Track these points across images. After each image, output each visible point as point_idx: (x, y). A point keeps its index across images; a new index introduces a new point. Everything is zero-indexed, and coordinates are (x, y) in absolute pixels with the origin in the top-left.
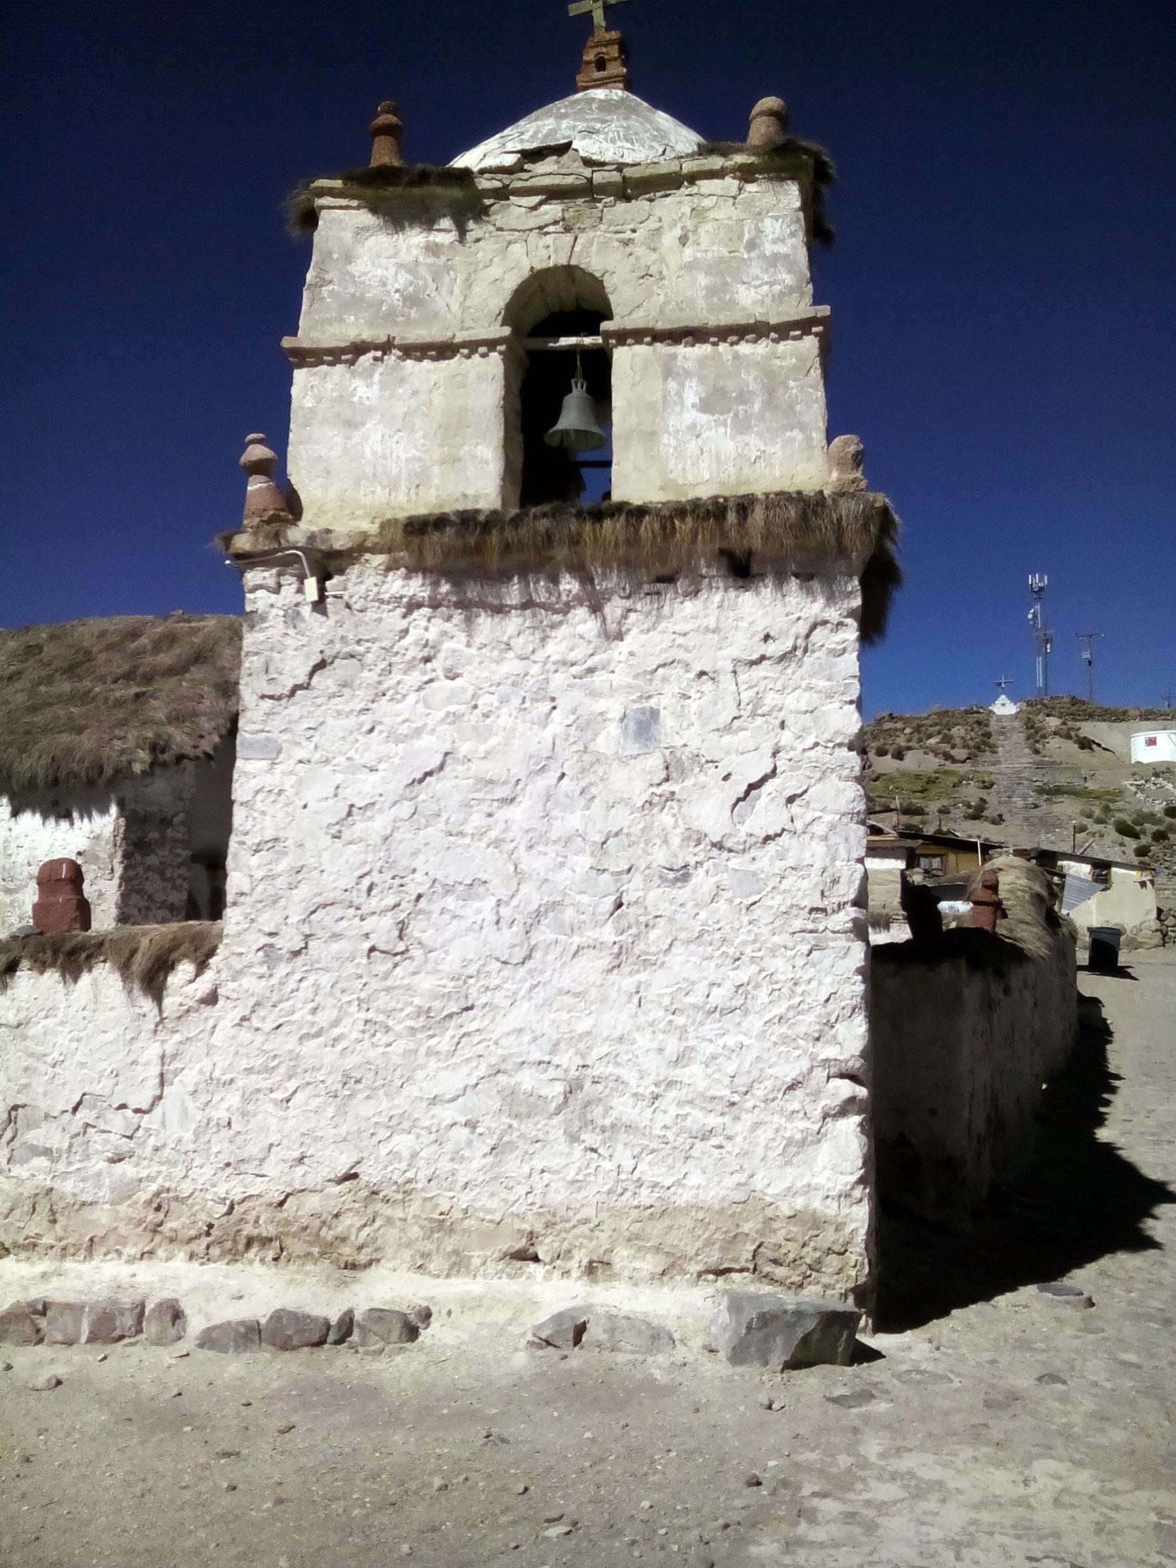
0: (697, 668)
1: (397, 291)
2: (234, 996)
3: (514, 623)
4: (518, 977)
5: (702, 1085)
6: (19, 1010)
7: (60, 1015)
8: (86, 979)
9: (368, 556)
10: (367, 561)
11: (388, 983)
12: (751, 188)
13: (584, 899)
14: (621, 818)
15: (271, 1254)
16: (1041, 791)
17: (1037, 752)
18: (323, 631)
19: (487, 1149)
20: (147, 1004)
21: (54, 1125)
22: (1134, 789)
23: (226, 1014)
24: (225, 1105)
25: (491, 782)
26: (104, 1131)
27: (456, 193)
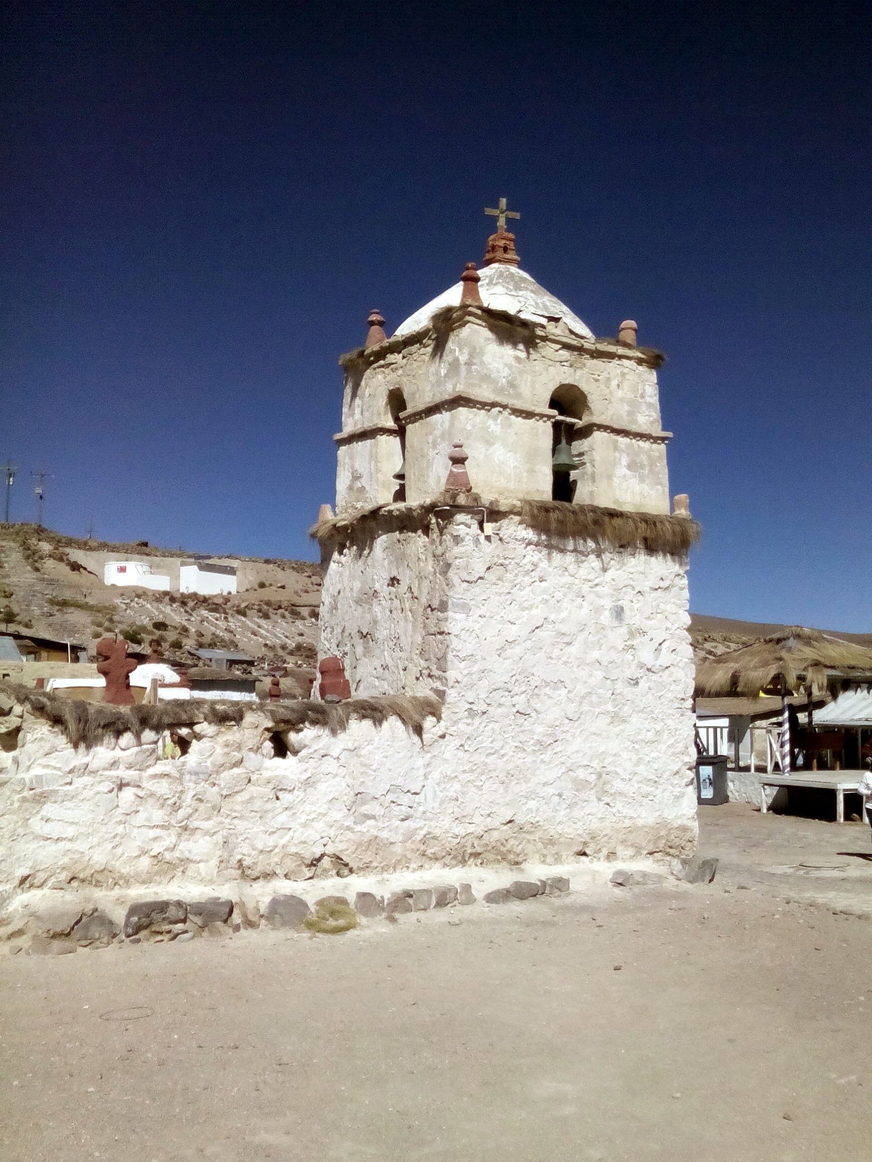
0: (637, 589)
1: (504, 377)
2: (455, 734)
3: (570, 558)
4: (576, 726)
5: (645, 774)
6: (355, 741)
7: (376, 744)
8: (385, 724)
9: (512, 516)
10: (511, 518)
11: (522, 728)
12: (640, 368)
13: (601, 691)
14: (614, 656)
15: (479, 861)
16: (52, 602)
17: (37, 570)
18: (489, 550)
19: (567, 806)
20: (416, 738)
21: (375, 803)
22: (124, 607)
23: (451, 744)
24: (453, 789)
25: (563, 634)
26: (399, 805)
27: (526, 332)
